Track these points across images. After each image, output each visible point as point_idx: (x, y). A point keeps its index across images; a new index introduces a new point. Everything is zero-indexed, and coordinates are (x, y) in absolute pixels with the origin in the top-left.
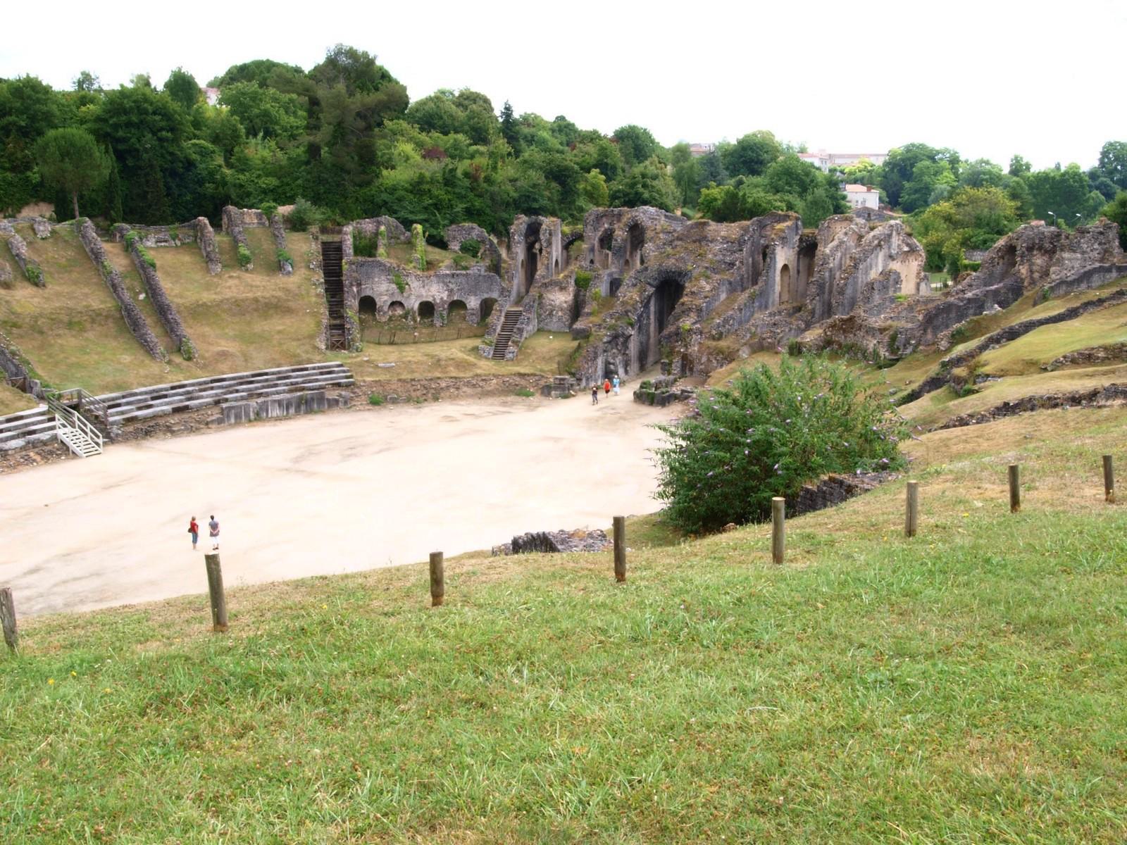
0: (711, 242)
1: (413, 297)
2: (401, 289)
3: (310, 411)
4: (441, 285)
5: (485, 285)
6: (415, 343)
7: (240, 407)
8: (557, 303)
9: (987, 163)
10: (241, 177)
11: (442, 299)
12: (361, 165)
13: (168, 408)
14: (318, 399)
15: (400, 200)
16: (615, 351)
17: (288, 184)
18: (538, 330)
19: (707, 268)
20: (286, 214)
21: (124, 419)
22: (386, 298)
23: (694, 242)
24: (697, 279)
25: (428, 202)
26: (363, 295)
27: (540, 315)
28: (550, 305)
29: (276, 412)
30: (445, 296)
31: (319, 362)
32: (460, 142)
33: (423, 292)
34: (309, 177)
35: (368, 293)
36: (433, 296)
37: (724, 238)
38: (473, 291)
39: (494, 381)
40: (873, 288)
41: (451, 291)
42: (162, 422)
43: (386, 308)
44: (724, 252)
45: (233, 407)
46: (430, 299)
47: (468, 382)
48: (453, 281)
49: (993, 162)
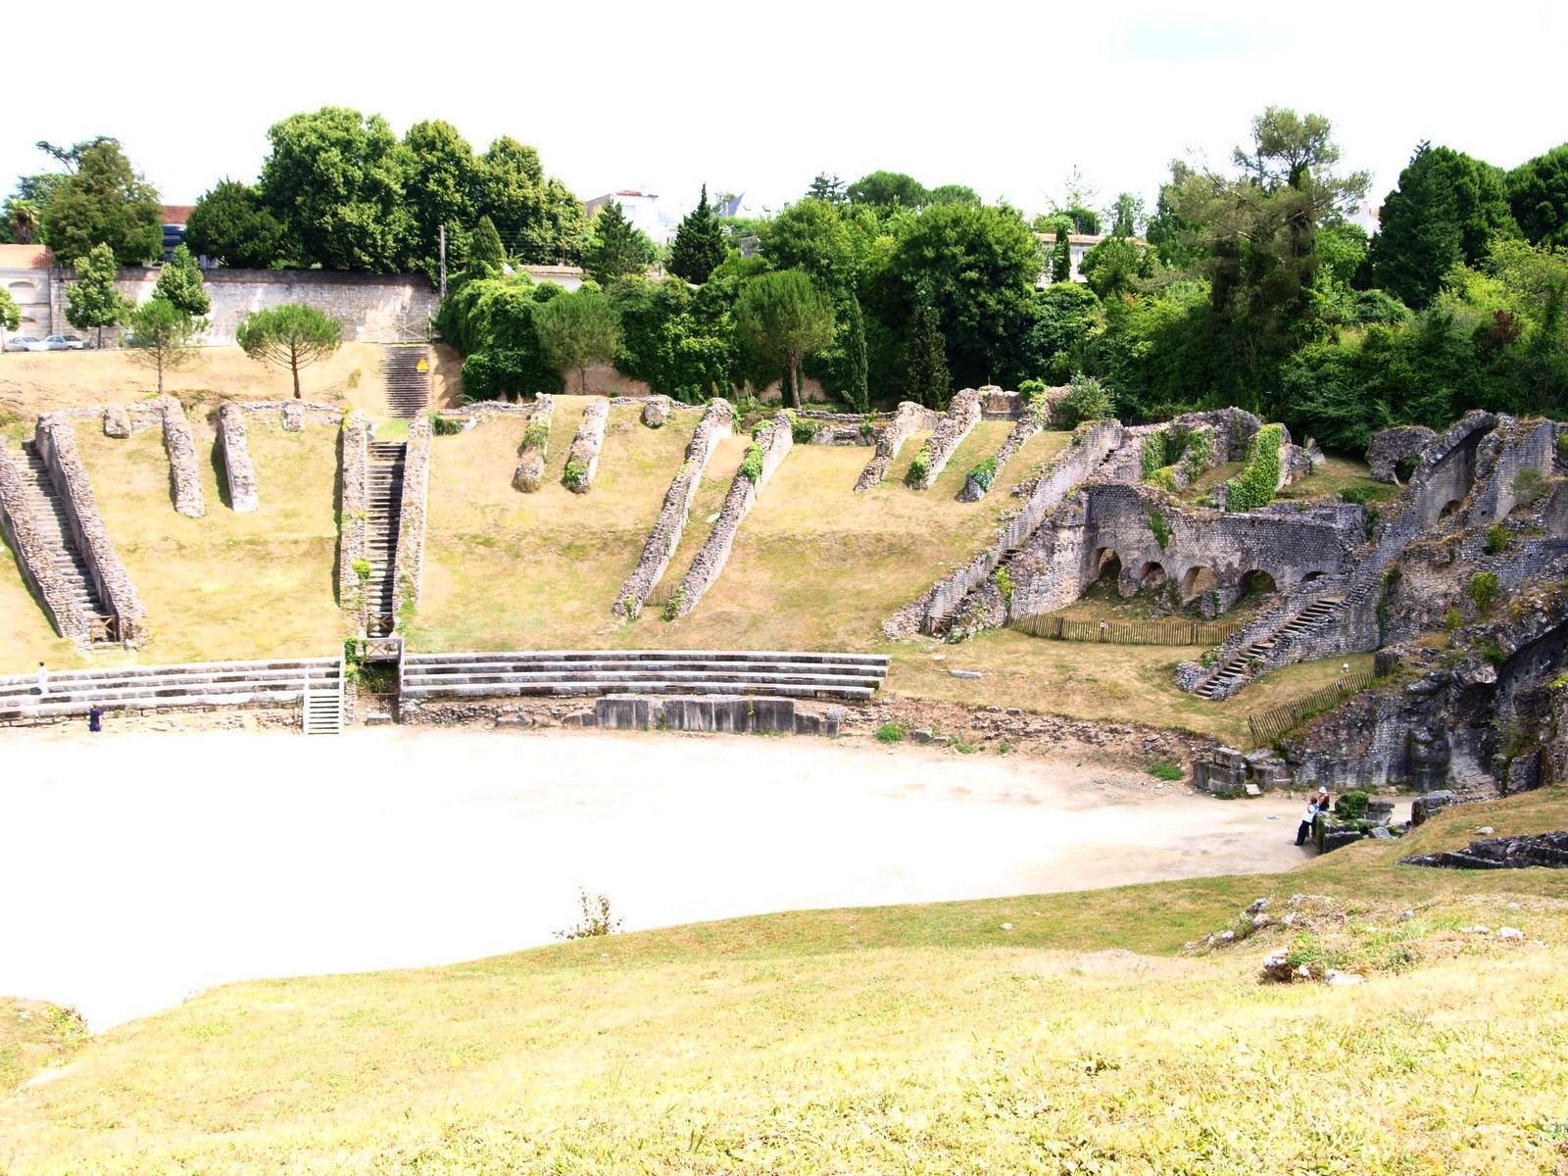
1: (1178, 557)
3: (760, 729)
4: (1230, 538)
7: (629, 703)
9: (967, 196)
11: (1230, 565)
13: (516, 687)
14: (780, 713)
21: (429, 692)
22: (1136, 554)
25: (1376, 381)
27: (1389, 617)
28: (1411, 597)
29: (699, 721)
30: (1235, 559)
31: (857, 651)
36: (1213, 559)
39: (1132, 737)
41: (1247, 553)
42: (491, 704)
43: (1135, 574)
45: (615, 702)
47: (1084, 730)
49: (929, 180)
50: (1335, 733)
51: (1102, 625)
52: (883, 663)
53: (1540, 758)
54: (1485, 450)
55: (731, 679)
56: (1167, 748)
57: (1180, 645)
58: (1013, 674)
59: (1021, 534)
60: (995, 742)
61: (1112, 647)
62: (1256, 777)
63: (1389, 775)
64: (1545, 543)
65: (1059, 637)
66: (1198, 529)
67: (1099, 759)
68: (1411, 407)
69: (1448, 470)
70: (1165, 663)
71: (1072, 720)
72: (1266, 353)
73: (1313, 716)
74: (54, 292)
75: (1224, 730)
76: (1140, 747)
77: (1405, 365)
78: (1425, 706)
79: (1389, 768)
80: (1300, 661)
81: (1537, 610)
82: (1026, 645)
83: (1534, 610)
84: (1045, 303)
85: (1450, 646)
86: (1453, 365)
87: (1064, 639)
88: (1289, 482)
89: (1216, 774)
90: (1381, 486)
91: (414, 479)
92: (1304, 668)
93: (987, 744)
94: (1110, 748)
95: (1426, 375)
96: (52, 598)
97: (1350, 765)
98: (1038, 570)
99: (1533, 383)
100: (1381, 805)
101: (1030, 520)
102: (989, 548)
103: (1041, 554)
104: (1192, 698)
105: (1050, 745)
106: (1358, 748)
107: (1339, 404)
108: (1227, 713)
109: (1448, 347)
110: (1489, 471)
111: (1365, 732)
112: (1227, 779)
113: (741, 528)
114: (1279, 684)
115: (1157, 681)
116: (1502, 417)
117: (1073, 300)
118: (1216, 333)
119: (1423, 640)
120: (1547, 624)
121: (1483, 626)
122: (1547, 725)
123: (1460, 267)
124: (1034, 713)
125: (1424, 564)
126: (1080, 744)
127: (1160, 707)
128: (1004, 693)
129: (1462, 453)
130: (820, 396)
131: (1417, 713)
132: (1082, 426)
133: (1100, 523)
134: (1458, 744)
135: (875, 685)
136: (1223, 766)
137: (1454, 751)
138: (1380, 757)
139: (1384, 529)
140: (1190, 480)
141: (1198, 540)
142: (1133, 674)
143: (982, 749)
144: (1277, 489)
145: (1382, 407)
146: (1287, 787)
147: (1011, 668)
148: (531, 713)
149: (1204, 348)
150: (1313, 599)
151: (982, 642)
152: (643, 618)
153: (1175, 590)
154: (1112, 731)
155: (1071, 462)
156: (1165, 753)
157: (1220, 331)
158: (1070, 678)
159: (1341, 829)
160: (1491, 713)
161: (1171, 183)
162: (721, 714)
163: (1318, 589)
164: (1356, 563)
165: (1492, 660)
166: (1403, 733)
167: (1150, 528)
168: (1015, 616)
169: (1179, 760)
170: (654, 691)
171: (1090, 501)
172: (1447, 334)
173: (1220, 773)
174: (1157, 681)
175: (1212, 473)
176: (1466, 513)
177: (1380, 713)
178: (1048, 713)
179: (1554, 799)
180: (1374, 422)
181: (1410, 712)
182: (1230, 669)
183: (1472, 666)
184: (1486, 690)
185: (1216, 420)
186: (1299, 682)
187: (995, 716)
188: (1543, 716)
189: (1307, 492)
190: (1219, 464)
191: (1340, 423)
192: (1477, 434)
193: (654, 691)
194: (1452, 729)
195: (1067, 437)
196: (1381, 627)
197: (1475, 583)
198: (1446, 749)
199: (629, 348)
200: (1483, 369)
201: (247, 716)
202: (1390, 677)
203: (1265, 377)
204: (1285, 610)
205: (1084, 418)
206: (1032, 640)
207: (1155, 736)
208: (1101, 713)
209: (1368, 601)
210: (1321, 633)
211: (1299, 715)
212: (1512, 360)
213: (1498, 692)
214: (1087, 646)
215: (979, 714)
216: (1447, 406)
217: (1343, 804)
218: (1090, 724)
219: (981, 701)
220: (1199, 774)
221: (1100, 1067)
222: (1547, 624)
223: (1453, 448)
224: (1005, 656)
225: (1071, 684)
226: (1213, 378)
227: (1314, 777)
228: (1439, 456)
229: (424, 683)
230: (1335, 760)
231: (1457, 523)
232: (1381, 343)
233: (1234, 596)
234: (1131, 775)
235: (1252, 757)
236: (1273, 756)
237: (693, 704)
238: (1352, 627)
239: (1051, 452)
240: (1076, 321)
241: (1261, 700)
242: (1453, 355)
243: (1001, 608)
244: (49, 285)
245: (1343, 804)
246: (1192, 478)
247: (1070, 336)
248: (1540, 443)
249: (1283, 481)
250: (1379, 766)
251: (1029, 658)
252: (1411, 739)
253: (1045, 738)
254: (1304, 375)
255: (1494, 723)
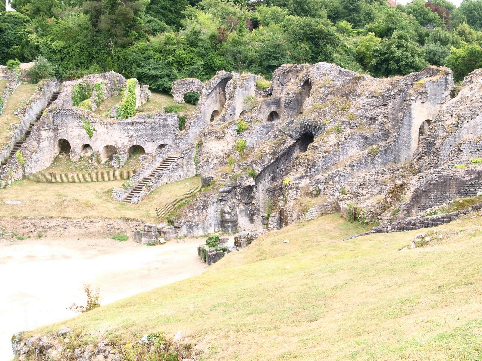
0: (359, 96)
1: (99, 141)
2: (90, 133)
4: (123, 131)
5: (161, 132)
6: (72, 182)
8: (214, 151)
10: (40, 40)
11: (123, 144)
12: (124, 30)
15: (148, 58)
16: (234, 200)
17: (70, 46)
18: (197, 175)
19: (343, 122)
20: (27, 69)
22: (78, 141)
23: (342, 96)
24: (328, 134)
25: (171, 58)
26: (59, 138)
27: (199, 162)
28: (208, 153)
30: (126, 141)
32: (277, 12)
33: (107, 137)
34: (85, 40)
35: (63, 136)
36: (115, 141)
37: (371, 93)
38: (150, 138)
40: (461, 150)
44: (368, 107)
46: (113, 144)
48: (132, 128)
50: (193, 212)
51: (72, 175)
53: (282, 213)
54: (229, 89)
56: (119, 227)
57: (109, 181)
58: (36, 201)
59: (21, 134)
60: (35, 233)
61: (77, 184)
62: (162, 235)
63: (215, 228)
64: (263, 126)
65: (51, 182)
66: (107, 128)
67: (89, 235)
68: (186, 70)
69: (213, 97)
70: (107, 190)
71: (70, 218)
72: (119, 46)
73: (182, 206)
75: (143, 216)
76: (105, 228)
77: (182, 51)
78: (226, 197)
79: (215, 225)
80: (166, 183)
81: (267, 154)
82: (37, 187)
83: (266, 154)
84: (5, 22)
85: (233, 171)
86: (203, 51)
87: (53, 183)
88: (140, 105)
89: (145, 235)
90: (180, 105)
92: (170, 187)
93: (31, 234)
94: (92, 230)
95: (192, 56)
97: (199, 226)
98: (34, 151)
99: (236, 59)
100: (224, 239)
101: (24, 128)
102: (8, 142)
103: (35, 143)
104: (122, 204)
105: (62, 232)
106: (202, 218)
107: (155, 69)
108: (141, 209)
109: (200, 44)
110: (232, 97)
111: (204, 211)
112: (151, 237)
114: (161, 194)
115: (105, 198)
116: (234, 73)
117: (19, 21)
118: (93, 37)
119: (220, 169)
120: (272, 159)
121: (246, 162)
122: (282, 200)
123: (189, 7)
124: (51, 217)
125: (213, 138)
126: (76, 230)
127: (111, 209)
128: (34, 210)
129: (218, 89)
131: (224, 200)
132: (41, 82)
133: (59, 127)
134: (241, 212)
136: (148, 231)
137: (239, 216)
138: (211, 221)
139: (190, 123)
140: (97, 105)
141: (107, 132)
142: (93, 196)
143: (29, 237)
144: (136, 108)
145: (175, 71)
146: (177, 238)
147: (35, 198)
149: (89, 44)
150: (166, 156)
151: (15, 187)
153: (98, 156)
154: (91, 222)
155: (39, 99)
156: (118, 229)
157: (95, 36)
158: (65, 200)
159: (214, 251)
160: (252, 198)
163: (167, 151)
164: (181, 139)
165: (253, 175)
166: (219, 210)
167: (84, 128)
168: (27, 174)
169: (125, 232)
171: (53, 117)
172: (200, 38)
173: (147, 235)
174: (105, 198)
175: (106, 102)
176: (225, 115)
177: (210, 202)
178: (59, 217)
179: (300, 227)
180: (172, 78)
181: (221, 200)
182: (137, 189)
183: (245, 179)
184: (250, 188)
185: (105, 77)
186: (170, 192)
187: (33, 221)
188: (279, 196)
189: (149, 109)
190: (108, 98)
191: (156, 78)
192: (224, 81)
194: (238, 206)
195: (36, 87)
196: (196, 166)
197: (238, 144)
198: (236, 215)
200: (215, 53)
202: (211, 186)
203: (119, 57)
204: (155, 161)
205: (41, 78)
206: (38, 184)
207: (112, 223)
208: (84, 215)
209: (191, 155)
210: (173, 170)
211: (177, 206)
212: (227, 49)
213: (254, 189)
214: (66, 185)
215: (25, 221)
216: (202, 69)
217: (209, 241)
218: (80, 220)
219: (24, 215)
220: (137, 237)
221: (478, 350)
222: (272, 159)
223: (215, 87)
224: (30, 193)
225: (65, 203)
226: (93, 58)
227: (186, 232)
228: (210, 91)
230: (194, 224)
231: (221, 120)
232: (171, 42)
233: (126, 158)
234: (104, 241)
235: (160, 226)
236: (168, 225)
238: (185, 167)
239: (29, 95)
240: (21, 31)
241: (155, 201)
242: (202, 46)
243: (21, 170)
245: (209, 241)
246: (98, 105)
247: (20, 38)
248: (250, 84)
249: (138, 105)
250: (210, 225)
251: (41, 192)
252: (223, 212)
253: (59, 229)
254: (138, 56)
255: (253, 202)
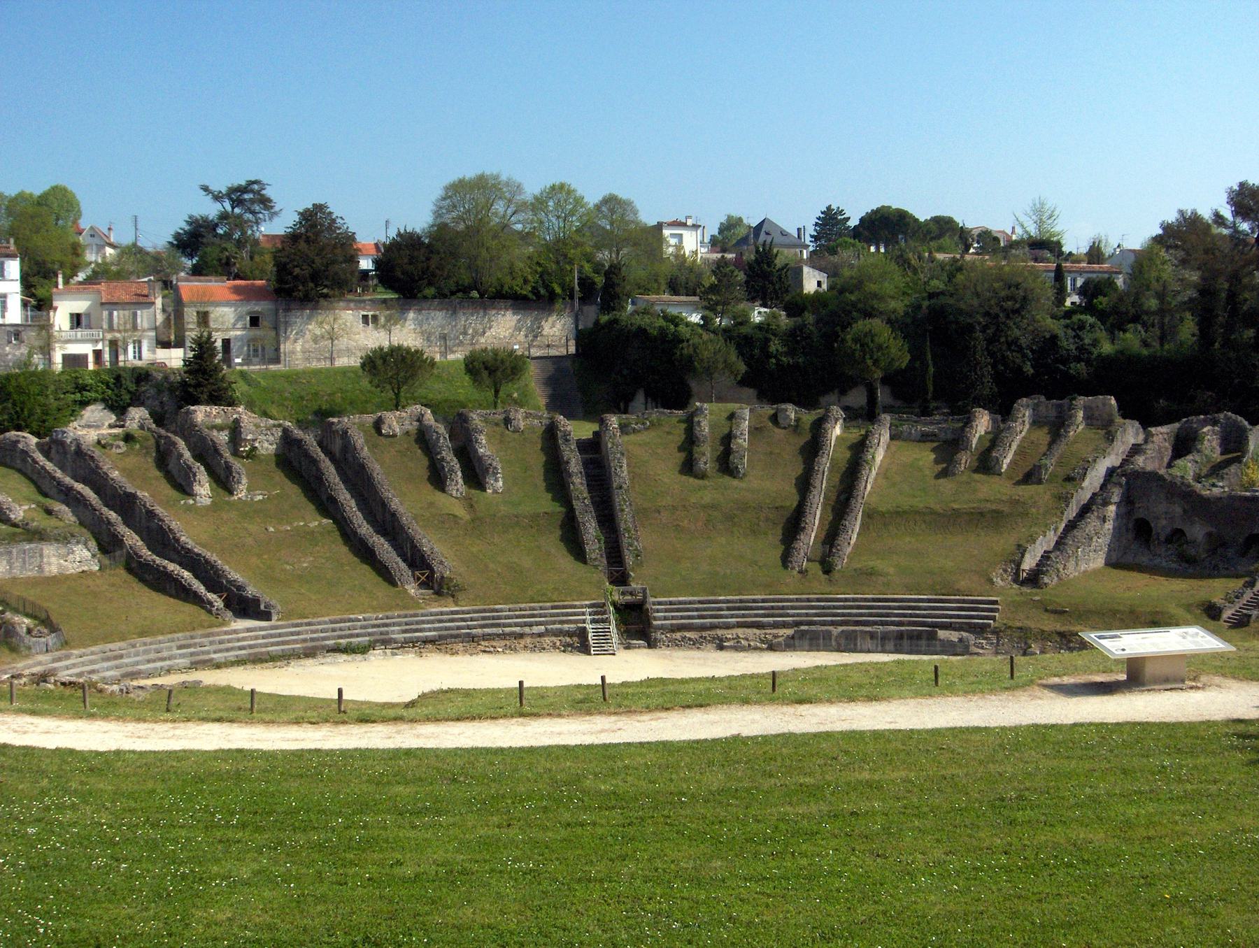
22: (1164, 522)
52: (995, 602)
55: (888, 615)
74: (502, 330)
91: (178, 732)
96: (475, 712)
113: (1104, 520)
130: (1140, 461)
135: (994, 618)
148: (747, 639)
152: (777, 430)
161: (263, 192)
162: (885, 637)
170: (833, 623)
193: (833, 623)
199: (765, 306)
201: (547, 640)
227: (1217, 456)
229: (665, 618)
237: (862, 632)
244: (534, 298)
